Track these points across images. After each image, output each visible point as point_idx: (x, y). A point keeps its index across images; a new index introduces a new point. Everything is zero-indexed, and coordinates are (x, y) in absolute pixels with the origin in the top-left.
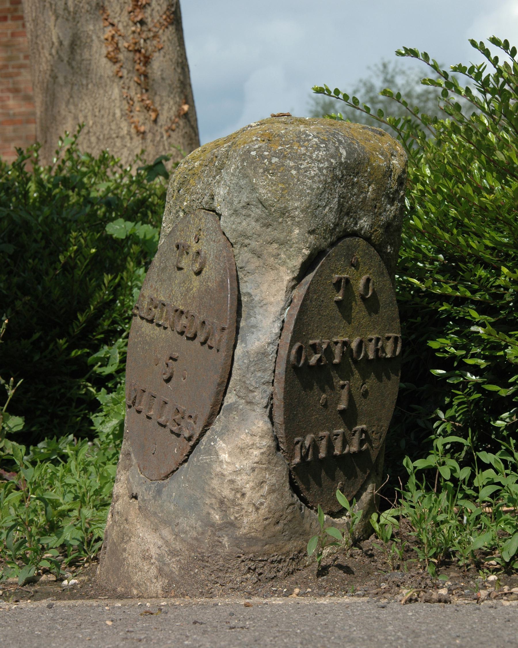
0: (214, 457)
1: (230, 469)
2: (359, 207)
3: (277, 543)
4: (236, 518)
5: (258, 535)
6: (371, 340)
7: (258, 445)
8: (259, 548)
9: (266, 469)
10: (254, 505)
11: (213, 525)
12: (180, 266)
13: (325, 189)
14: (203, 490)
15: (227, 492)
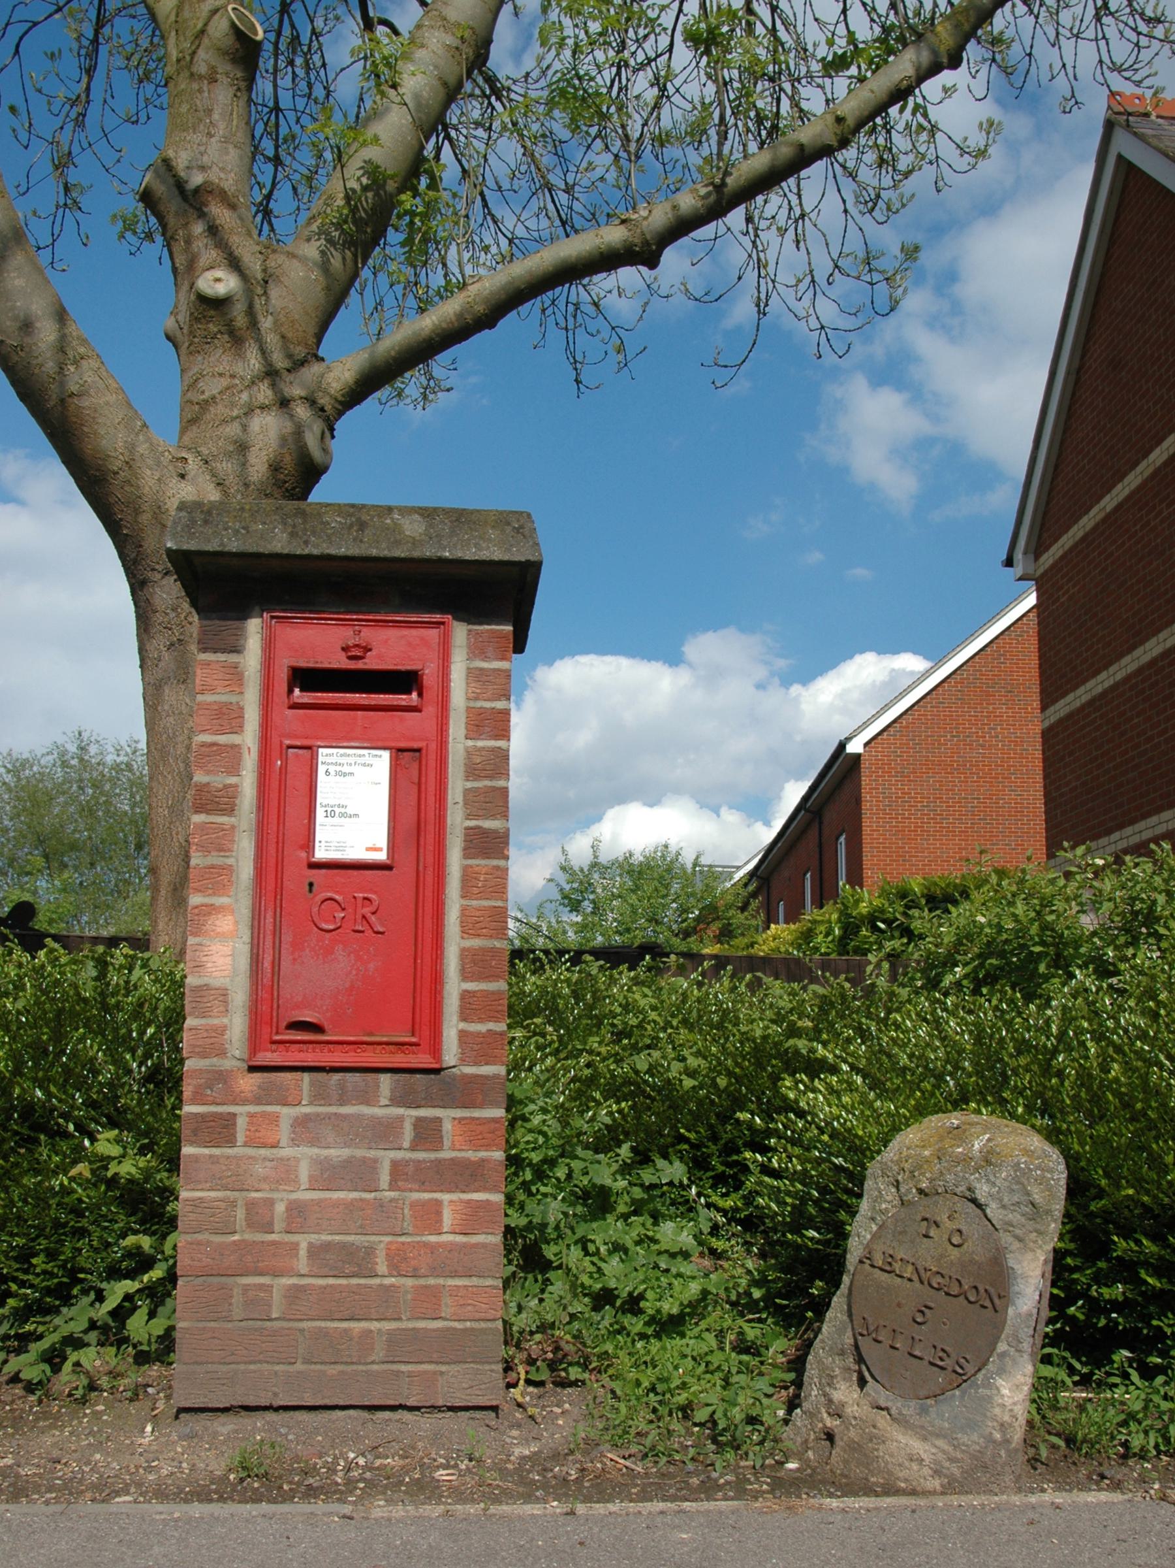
0: (995, 1392)
1: (1011, 1401)
11: (995, 1442)
12: (925, 1223)
14: (985, 1416)
15: (1006, 1418)
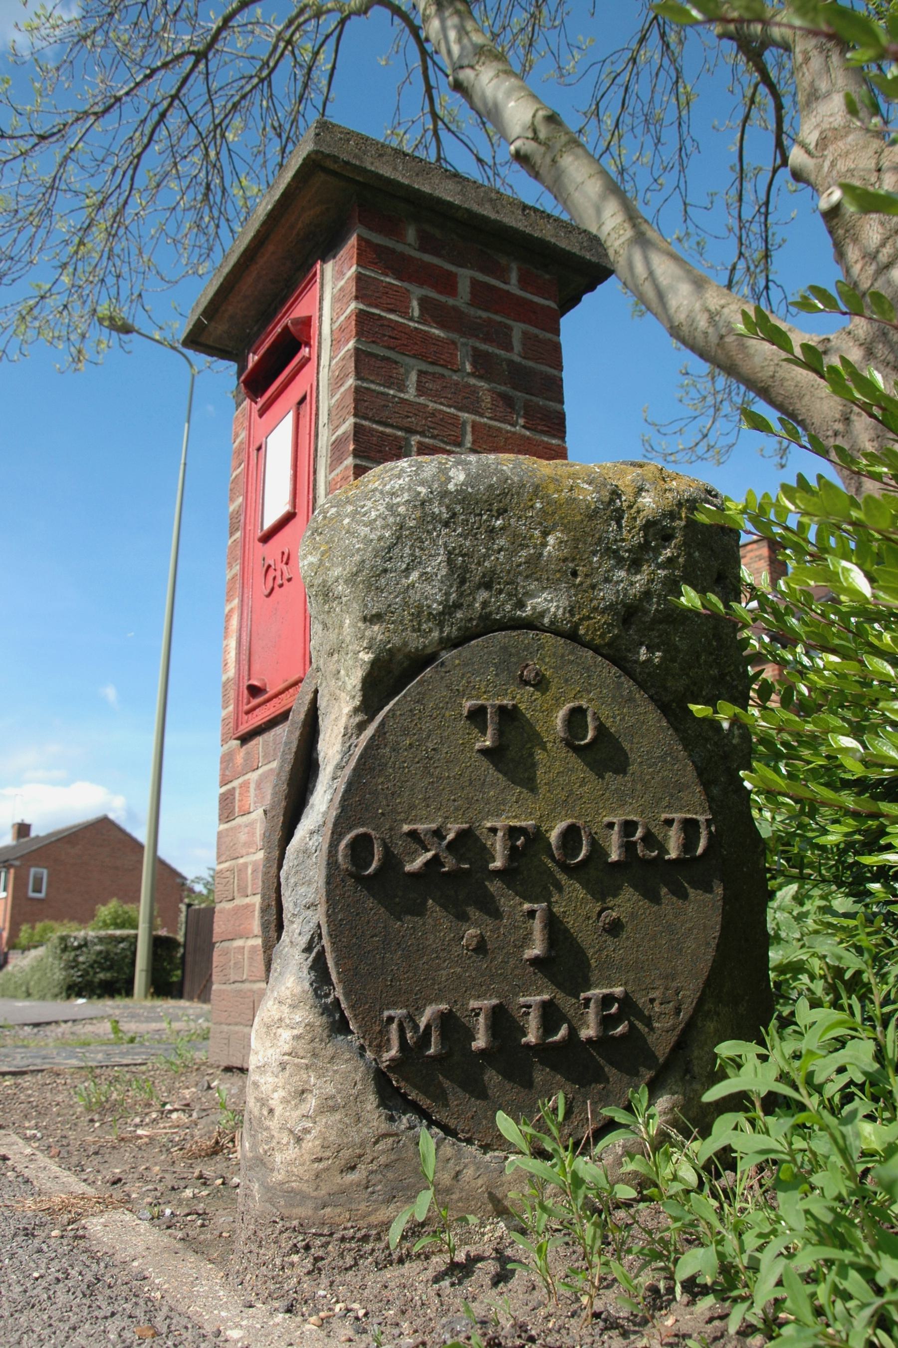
2: (520, 573)
3: (353, 1207)
4: (266, 1152)
5: (305, 1187)
6: (611, 825)
7: (288, 1021)
8: (310, 1213)
9: (307, 1067)
10: (291, 1132)
13: (398, 538)
